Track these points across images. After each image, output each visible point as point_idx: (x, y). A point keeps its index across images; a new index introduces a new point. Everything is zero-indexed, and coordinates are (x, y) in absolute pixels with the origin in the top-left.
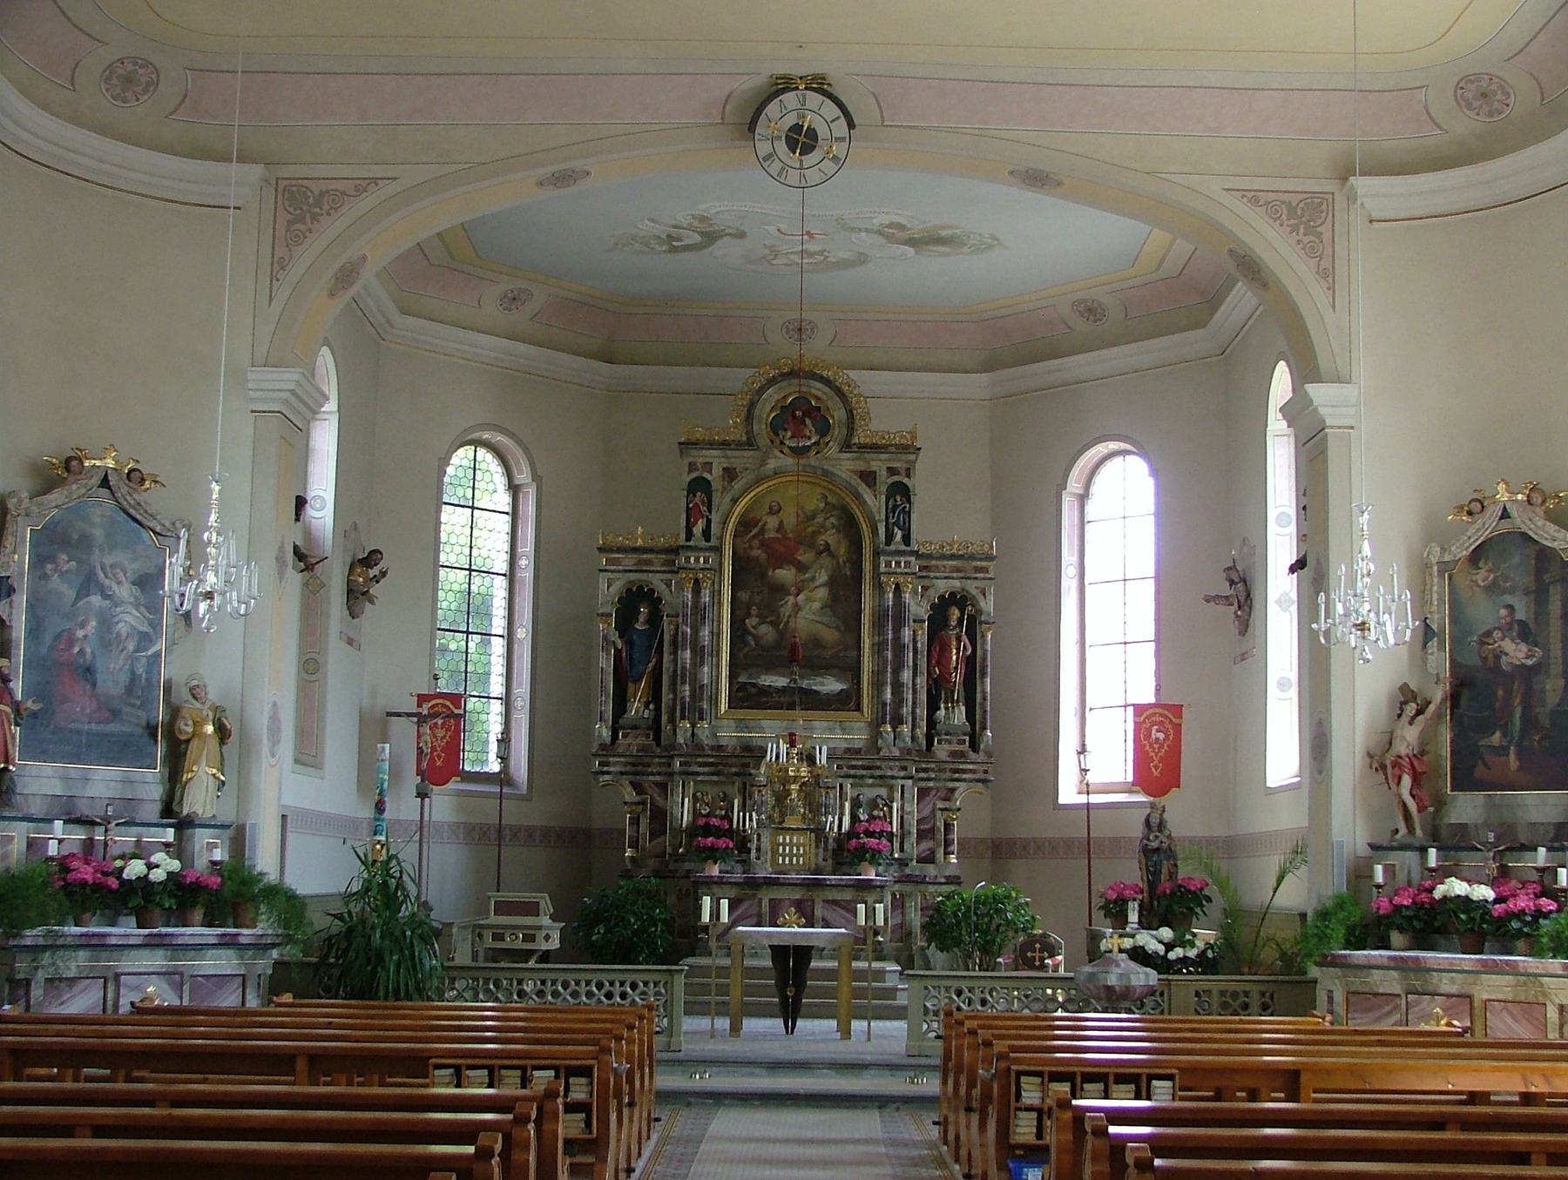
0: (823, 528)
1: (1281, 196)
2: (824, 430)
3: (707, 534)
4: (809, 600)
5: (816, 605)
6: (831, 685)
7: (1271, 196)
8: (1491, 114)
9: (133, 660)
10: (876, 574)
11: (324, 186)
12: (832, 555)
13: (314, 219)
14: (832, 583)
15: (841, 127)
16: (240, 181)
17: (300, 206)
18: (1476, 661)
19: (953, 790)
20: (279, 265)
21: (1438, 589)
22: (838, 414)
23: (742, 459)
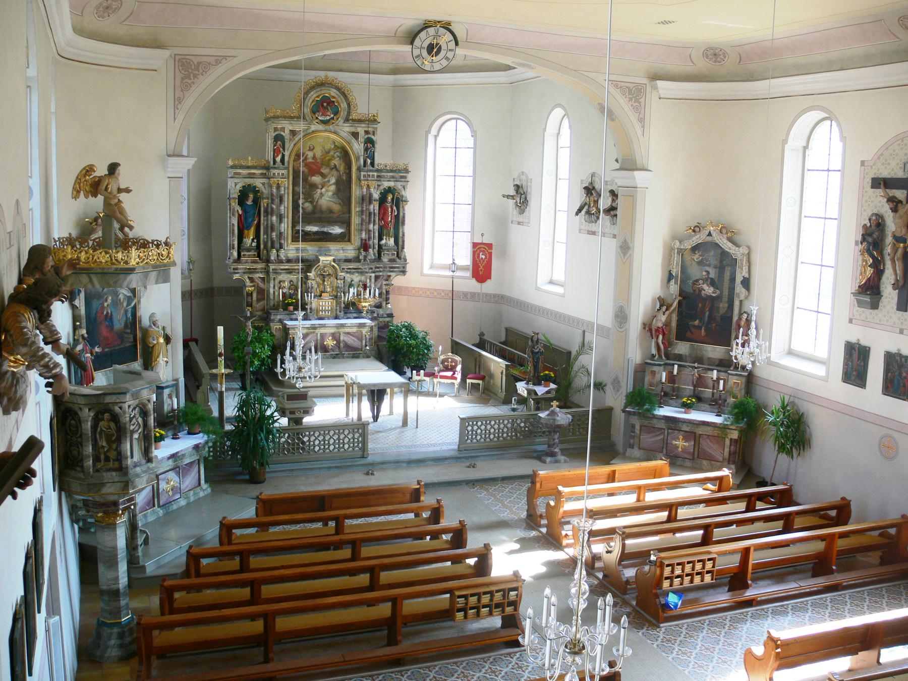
0: (333, 158)
2: (336, 113)
3: (282, 161)
4: (327, 191)
5: (330, 194)
6: (337, 230)
7: (623, 84)
8: (715, 62)
9: (126, 311)
10: (359, 179)
11: (199, 59)
12: (337, 170)
13: (195, 76)
14: (337, 183)
15: (452, 45)
16: (158, 58)
17: (188, 70)
19: (390, 276)
20: (178, 101)
21: (676, 259)
22: (344, 105)
23: (300, 126)
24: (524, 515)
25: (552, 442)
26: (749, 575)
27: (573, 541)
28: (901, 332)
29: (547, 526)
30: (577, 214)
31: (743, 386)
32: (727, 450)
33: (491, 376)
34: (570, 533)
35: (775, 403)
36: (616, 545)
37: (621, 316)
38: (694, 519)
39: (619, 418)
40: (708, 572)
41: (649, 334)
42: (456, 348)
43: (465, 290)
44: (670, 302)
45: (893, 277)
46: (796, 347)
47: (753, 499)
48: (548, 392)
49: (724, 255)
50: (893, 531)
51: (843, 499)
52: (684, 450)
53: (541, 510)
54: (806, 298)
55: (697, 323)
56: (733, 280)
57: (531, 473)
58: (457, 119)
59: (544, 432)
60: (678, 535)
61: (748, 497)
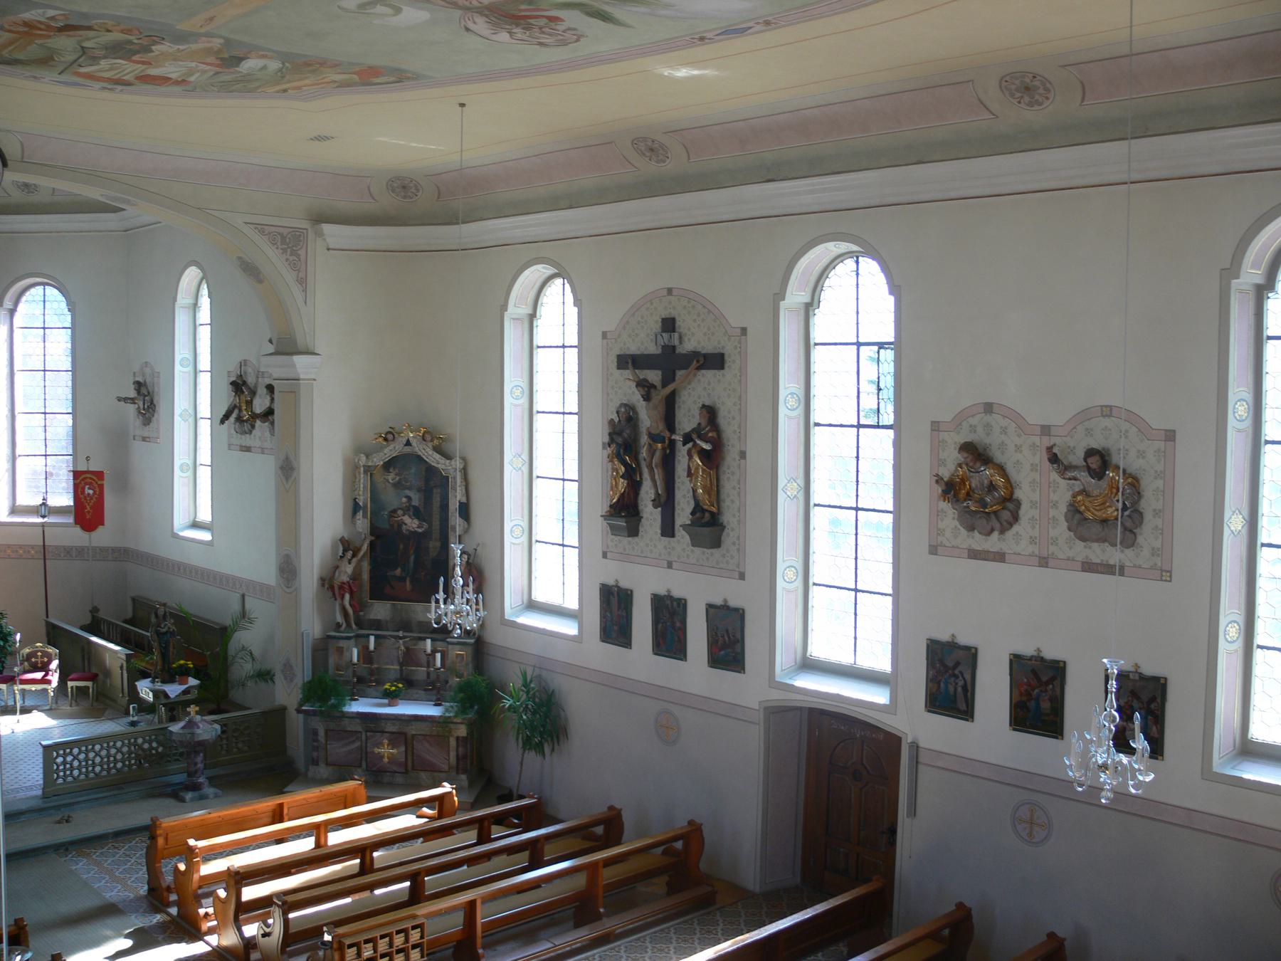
1: (278, 230)
7: (273, 229)
8: (405, 197)
18: (387, 526)
21: (363, 481)
24: (144, 890)
25: (192, 769)
26: (479, 941)
27: (215, 923)
28: (670, 565)
29: (178, 904)
30: (222, 422)
31: (470, 659)
32: (453, 754)
33: (107, 673)
34: (211, 910)
35: (515, 683)
36: (275, 922)
37: (288, 570)
38: (401, 864)
39: (296, 723)
40: (414, 947)
41: (330, 594)
42: (54, 635)
43: (67, 543)
44: (357, 545)
45: (653, 491)
46: (539, 596)
47: (486, 823)
48: (185, 692)
49: (431, 471)
50: (679, 845)
51: (611, 808)
52: (392, 759)
53: (169, 879)
54: (546, 527)
55: (398, 572)
56: (445, 507)
57: (149, 822)
58: (44, 284)
59: (182, 754)
60: (378, 892)
61: (480, 821)
